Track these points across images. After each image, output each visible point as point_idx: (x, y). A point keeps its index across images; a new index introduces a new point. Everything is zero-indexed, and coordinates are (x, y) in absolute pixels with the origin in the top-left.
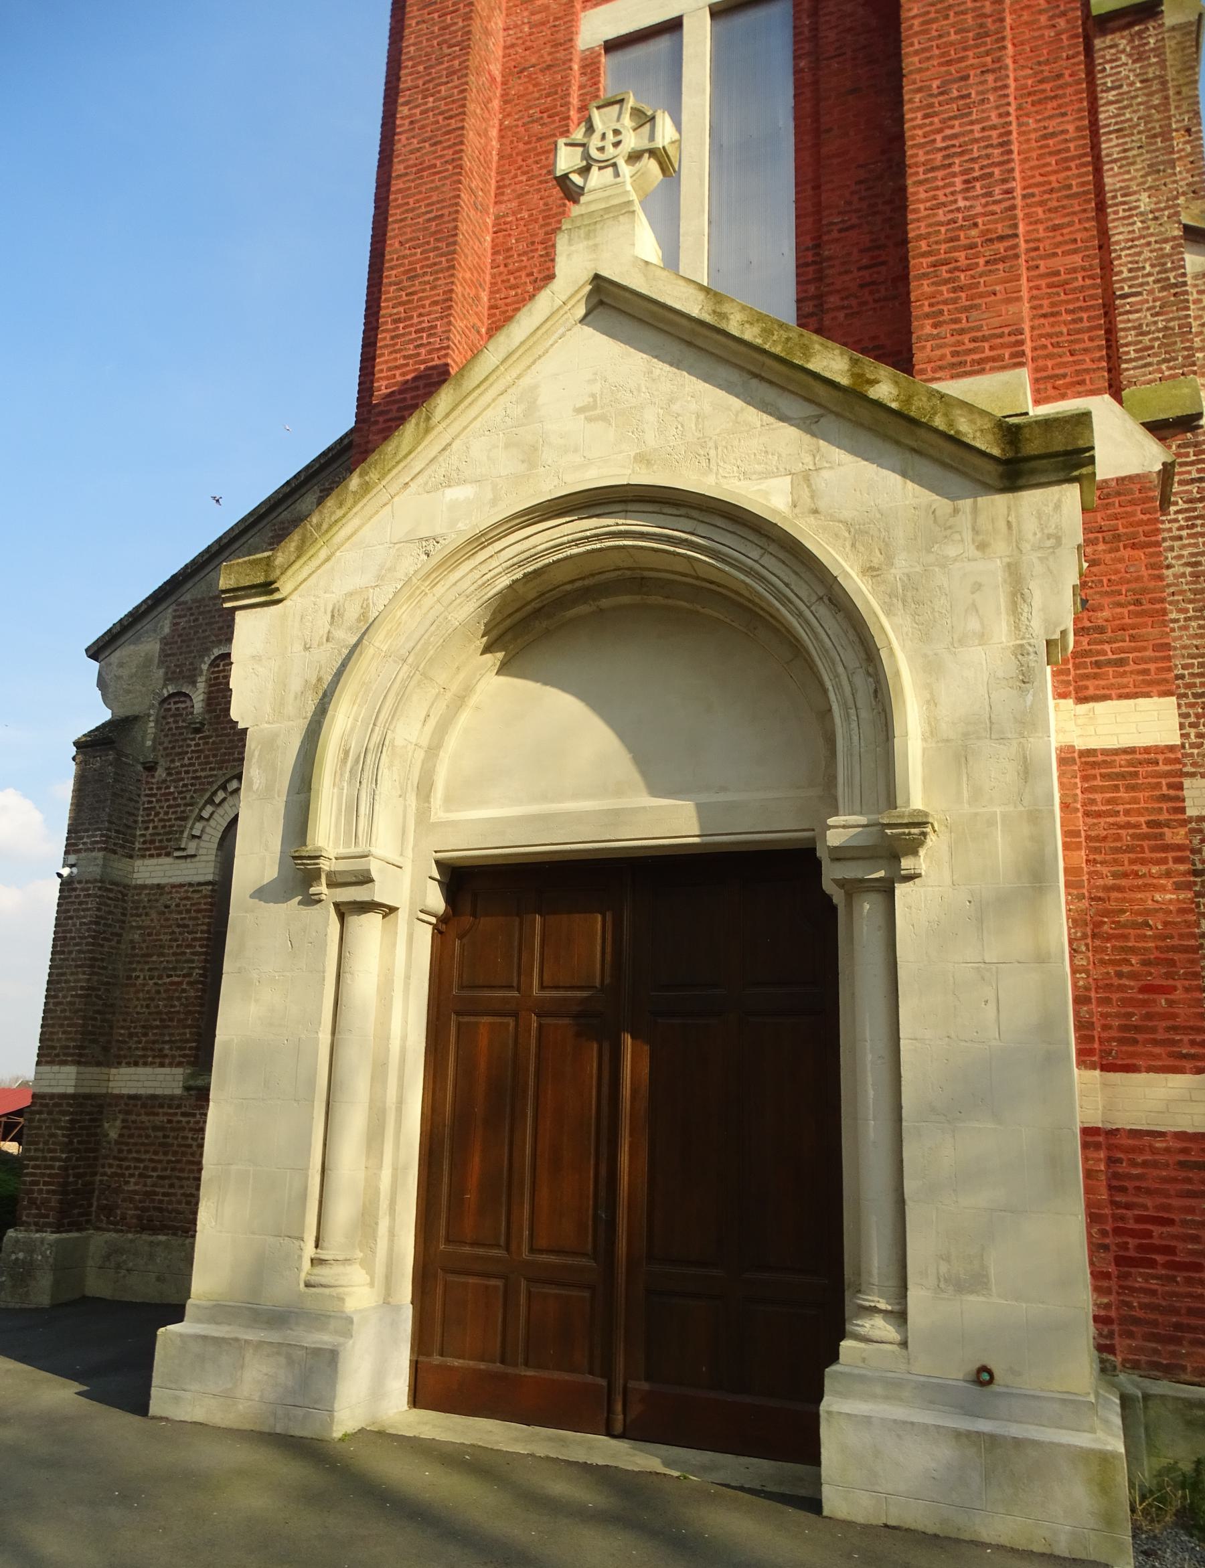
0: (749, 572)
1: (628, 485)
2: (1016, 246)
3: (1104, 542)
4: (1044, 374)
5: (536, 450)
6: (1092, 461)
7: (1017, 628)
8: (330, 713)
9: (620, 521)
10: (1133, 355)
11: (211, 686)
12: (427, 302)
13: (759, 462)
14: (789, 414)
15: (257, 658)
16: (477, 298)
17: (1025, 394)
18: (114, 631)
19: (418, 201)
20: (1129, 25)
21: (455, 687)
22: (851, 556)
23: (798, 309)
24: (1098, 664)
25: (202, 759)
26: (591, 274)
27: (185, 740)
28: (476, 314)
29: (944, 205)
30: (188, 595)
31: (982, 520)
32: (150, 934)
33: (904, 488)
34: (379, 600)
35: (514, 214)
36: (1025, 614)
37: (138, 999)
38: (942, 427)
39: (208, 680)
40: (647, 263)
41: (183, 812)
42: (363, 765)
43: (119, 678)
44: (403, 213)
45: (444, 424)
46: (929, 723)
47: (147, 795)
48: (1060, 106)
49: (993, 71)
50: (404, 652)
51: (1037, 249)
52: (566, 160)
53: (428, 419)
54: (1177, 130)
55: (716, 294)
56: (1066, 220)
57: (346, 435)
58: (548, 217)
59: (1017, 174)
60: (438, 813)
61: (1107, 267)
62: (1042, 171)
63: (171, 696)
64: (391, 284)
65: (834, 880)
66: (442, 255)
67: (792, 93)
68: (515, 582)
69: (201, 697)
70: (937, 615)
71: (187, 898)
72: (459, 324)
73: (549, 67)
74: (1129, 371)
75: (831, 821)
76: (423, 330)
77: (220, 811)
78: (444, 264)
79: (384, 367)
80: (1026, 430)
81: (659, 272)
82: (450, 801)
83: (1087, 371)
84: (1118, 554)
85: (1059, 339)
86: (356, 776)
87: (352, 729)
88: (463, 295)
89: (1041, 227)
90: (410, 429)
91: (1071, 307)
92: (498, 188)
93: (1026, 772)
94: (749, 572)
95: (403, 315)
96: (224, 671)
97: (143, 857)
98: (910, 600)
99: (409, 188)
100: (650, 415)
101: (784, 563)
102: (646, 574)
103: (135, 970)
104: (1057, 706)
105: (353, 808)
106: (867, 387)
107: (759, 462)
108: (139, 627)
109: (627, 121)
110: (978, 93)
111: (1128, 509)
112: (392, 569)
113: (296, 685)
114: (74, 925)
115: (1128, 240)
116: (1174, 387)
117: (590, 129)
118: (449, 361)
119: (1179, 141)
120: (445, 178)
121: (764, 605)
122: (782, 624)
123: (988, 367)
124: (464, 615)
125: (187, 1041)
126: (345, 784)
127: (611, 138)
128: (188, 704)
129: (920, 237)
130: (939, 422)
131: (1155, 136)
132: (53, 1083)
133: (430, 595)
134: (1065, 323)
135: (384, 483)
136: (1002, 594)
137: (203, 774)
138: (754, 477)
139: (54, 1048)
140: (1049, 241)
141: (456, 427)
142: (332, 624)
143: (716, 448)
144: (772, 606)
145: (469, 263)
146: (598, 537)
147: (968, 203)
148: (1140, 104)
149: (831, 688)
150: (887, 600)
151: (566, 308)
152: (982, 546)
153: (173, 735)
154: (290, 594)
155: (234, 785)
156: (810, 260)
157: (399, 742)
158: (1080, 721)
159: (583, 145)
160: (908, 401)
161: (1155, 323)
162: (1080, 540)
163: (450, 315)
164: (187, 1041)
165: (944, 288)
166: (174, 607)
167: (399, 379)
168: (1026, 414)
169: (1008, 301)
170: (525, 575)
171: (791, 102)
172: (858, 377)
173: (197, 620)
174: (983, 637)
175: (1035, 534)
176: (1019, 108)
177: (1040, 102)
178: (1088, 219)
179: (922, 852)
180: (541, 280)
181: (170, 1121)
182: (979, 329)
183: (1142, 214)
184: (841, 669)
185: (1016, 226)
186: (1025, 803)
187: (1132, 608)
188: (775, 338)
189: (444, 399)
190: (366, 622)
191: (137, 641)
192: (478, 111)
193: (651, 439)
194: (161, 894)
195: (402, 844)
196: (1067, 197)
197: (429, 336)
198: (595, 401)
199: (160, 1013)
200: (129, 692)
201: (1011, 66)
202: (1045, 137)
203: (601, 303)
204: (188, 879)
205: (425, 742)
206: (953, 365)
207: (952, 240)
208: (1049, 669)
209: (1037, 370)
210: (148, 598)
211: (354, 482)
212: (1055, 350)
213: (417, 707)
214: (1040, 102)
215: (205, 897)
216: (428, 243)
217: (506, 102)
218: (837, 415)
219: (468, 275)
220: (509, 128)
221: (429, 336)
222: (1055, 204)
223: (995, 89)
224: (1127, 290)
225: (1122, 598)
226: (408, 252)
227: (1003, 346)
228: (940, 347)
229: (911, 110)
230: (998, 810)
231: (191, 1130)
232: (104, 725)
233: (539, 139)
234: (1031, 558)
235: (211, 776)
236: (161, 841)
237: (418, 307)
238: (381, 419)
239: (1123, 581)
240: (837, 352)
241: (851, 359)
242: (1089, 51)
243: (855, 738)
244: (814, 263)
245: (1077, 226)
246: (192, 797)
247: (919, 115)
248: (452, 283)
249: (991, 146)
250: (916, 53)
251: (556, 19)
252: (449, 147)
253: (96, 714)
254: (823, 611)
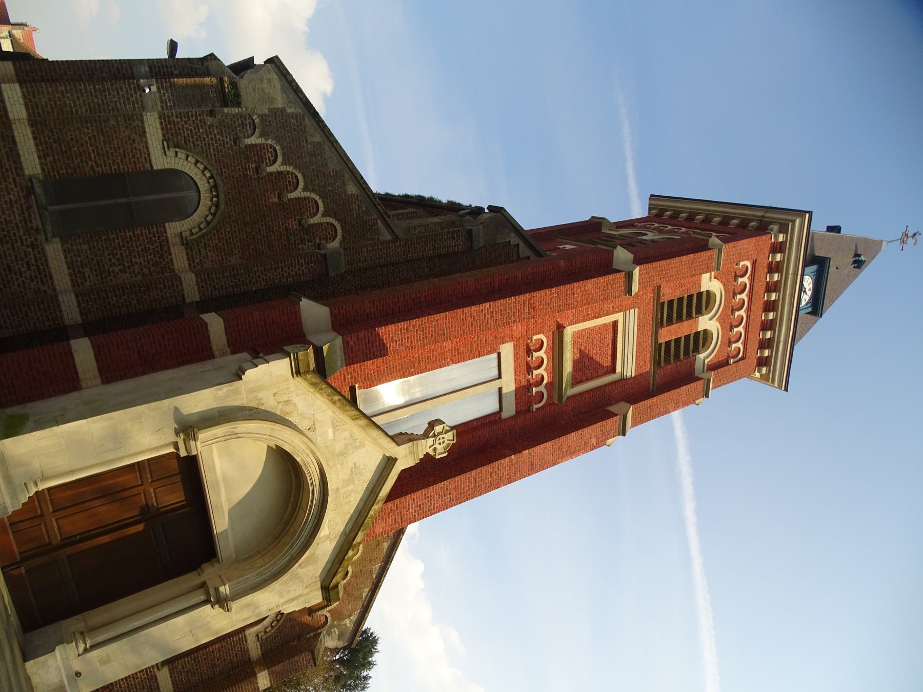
0: (300, 533)
32: (115, 131)
37: (75, 131)
63: (253, 120)
71: (141, 154)
94: (300, 533)
97: (160, 118)
103: (92, 125)
114: (114, 97)
125: (58, 172)
132: (12, 100)
139: (34, 97)
164: (58, 172)
166: (302, 113)
174: (281, 596)
181: (7, 170)
191: (283, 90)
193: (342, 491)
194: (140, 136)
199: (70, 149)
200: (254, 91)
204: (152, 152)
215: (144, 167)
231: (6, 186)
236: (171, 129)
254: (288, 558)
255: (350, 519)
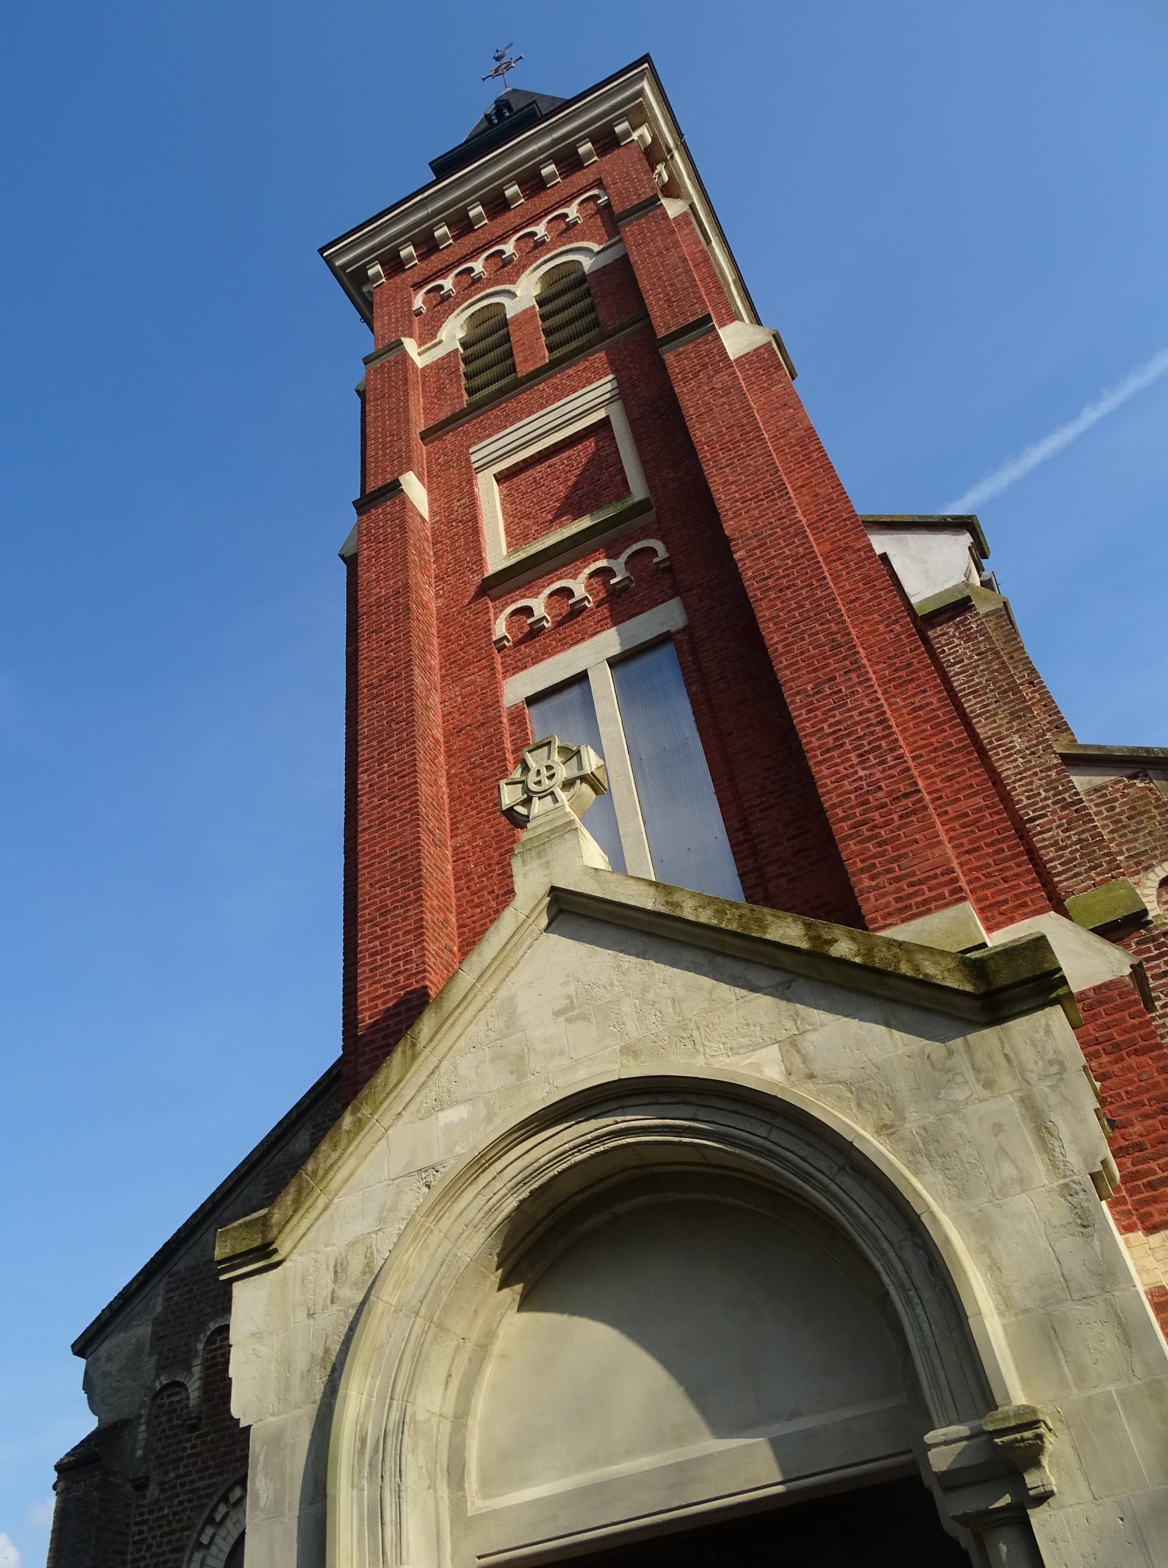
1: (620, 1080)
2: (921, 800)
3: (1107, 1054)
4: (988, 903)
5: (523, 1059)
6: (1063, 981)
7: (1055, 1166)
8: (341, 1392)
9: (619, 1119)
10: (1060, 868)
11: (207, 1368)
12: (400, 933)
13: (745, 1038)
14: (763, 984)
15: (257, 1336)
16: (446, 920)
17: (974, 921)
18: (104, 1318)
19: (383, 848)
20: (952, 618)
21: (474, 1335)
22: (859, 1115)
23: (742, 883)
24: (1151, 1186)
25: (200, 1465)
26: (549, 887)
27: (180, 1442)
28: (447, 935)
29: (847, 776)
30: (180, 1265)
31: (979, 1056)
33: (892, 1038)
34: (383, 1245)
35: (469, 843)
36: (1057, 1149)
38: (910, 973)
39: (205, 1361)
40: (596, 869)
41: (179, 1540)
42: (382, 1455)
43: (106, 1375)
44: (371, 859)
45: (429, 1048)
46: (1000, 1293)
47: (138, 1524)
48: (918, 686)
49: (854, 670)
50: (415, 1302)
51: (940, 798)
52: (509, 796)
53: (414, 1045)
54: (1022, 684)
55: (665, 887)
56: (958, 770)
57: (334, 1066)
58: (500, 841)
59: (901, 742)
60: (476, 1503)
61: (1006, 799)
62: (922, 736)
63: (164, 1388)
64: (365, 922)
65: (956, 1519)
66: (409, 890)
67: (691, 711)
68: (521, 1202)
69: (197, 1385)
70: (967, 1166)
72: (432, 947)
73: (483, 724)
74: (1063, 883)
75: (930, 1438)
76: (399, 959)
77: (223, 1532)
78: (413, 897)
79: (366, 998)
80: (991, 963)
81: (609, 876)
82: (488, 1485)
83: (1025, 893)
84: (1125, 1064)
85: (990, 870)
86: (377, 1473)
87: (367, 1408)
88: (433, 921)
89: (937, 780)
90: (397, 1057)
91: (989, 840)
92: (452, 824)
93: (1126, 1335)
95: (379, 948)
96: (221, 1347)
98: (934, 1155)
99: (374, 838)
100: (627, 1008)
101: (794, 1135)
102: (655, 1169)
104: (1127, 1242)
105: (376, 1515)
106: (827, 947)
107: (745, 1038)
108: (129, 1308)
109: (556, 757)
110: (847, 688)
111: (1116, 1016)
112: (393, 1209)
113: (301, 1362)
115: (1016, 774)
116: (1110, 890)
117: (526, 769)
118: (427, 983)
119: (1027, 692)
120: (405, 825)
121: (784, 1184)
122: (811, 1203)
123: (932, 906)
124: (474, 1250)
126: (365, 1483)
127: (544, 772)
128: (183, 1395)
129: (834, 806)
130: (905, 969)
131: (1005, 691)
133: (436, 1232)
134: (988, 855)
135: (376, 1117)
136: (1025, 1132)
137: (201, 1484)
138: (742, 1051)
140: (948, 790)
141: (441, 1049)
142: (335, 1281)
143: (698, 1028)
144: (795, 1184)
145: (434, 891)
146: (599, 1139)
147: (867, 772)
148: (982, 671)
149: (881, 1269)
150: (911, 1158)
151: (530, 921)
152: (988, 1084)
153: (167, 1438)
154: (289, 1254)
155: (237, 1492)
156: (742, 839)
157: (421, 1416)
158: (1158, 1255)
159: (522, 782)
160: (869, 953)
161: (1069, 837)
162: (1083, 1061)
163: (423, 941)
165: (870, 845)
166: (167, 1279)
167: (381, 1007)
168: (984, 945)
169: (931, 846)
170: (531, 1192)
171: (692, 718)
172: (815, 939)
173: (191, 1291)
174: (1023, 1183)
175: (1036, 1063)
176: (885, 692)
177: (901, 685)
178: (976, 767)
179: (1045, 1461)
180: (503, 895)
182: (913, 874)
183: (1019, 751)
184: (886, 1245)
185: (915, 783)
186: (1139, 1374)
187: (1161, 1117)
188: (729, 916)
189: (426, 1025)
190: (372, 1273)
192: (427, 767)
193: (634, 1030)
195: (439, 1554)
196: (951, 752)
197: (405, 963)
198: (572, 1002)
201: (867, 664)
202: (914, 710)
203: (561, 911)
205: (449, 1411)
206: (900, 911)
207: (863, 804)
208: (1104, 1203)
209: (978, 900)
210: (139, 1274)
211: (347, 1121)
212: (989, 880)
213: (436, 1370)
214: (901, 685)
216: (396, 881)
217: (449, 756)
218: (807, 977)
219: (435, 902)
220: (456, 775)
221: (405, 963)
222: (942, 760)
223: (860, 683)
224: (1032, 815)
225: (1147, 1109)
226: (378, 892)
227: (940, 885)
228: (883, 896)
229: (796, 709)
230: (1112, 1388)
232: (90, 1438)
233: (482, 780)
234: (1041, 1088)
235: (210, 1486)
237: (392, 938)
238: (367, 1049)
239: (1141, 1091)
240: (790, 920)
241: (804, 924)
242: (926, 641)
243: (925, 1326)
244: (746, 841)
245: (969, 774)
246: (189, 1518)
247: (803, 711)
248: (422, 912)
249: (872, 725)
250: (786, 667)
251: (483, 689)
252: (406, 799)
253: (83, 1423)
254: (848, 1182)
255: (735, 981)
